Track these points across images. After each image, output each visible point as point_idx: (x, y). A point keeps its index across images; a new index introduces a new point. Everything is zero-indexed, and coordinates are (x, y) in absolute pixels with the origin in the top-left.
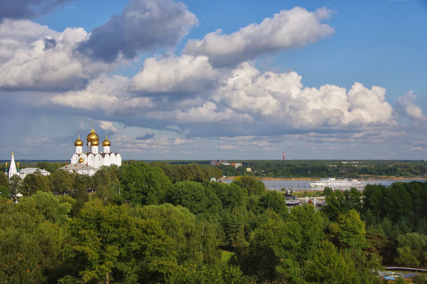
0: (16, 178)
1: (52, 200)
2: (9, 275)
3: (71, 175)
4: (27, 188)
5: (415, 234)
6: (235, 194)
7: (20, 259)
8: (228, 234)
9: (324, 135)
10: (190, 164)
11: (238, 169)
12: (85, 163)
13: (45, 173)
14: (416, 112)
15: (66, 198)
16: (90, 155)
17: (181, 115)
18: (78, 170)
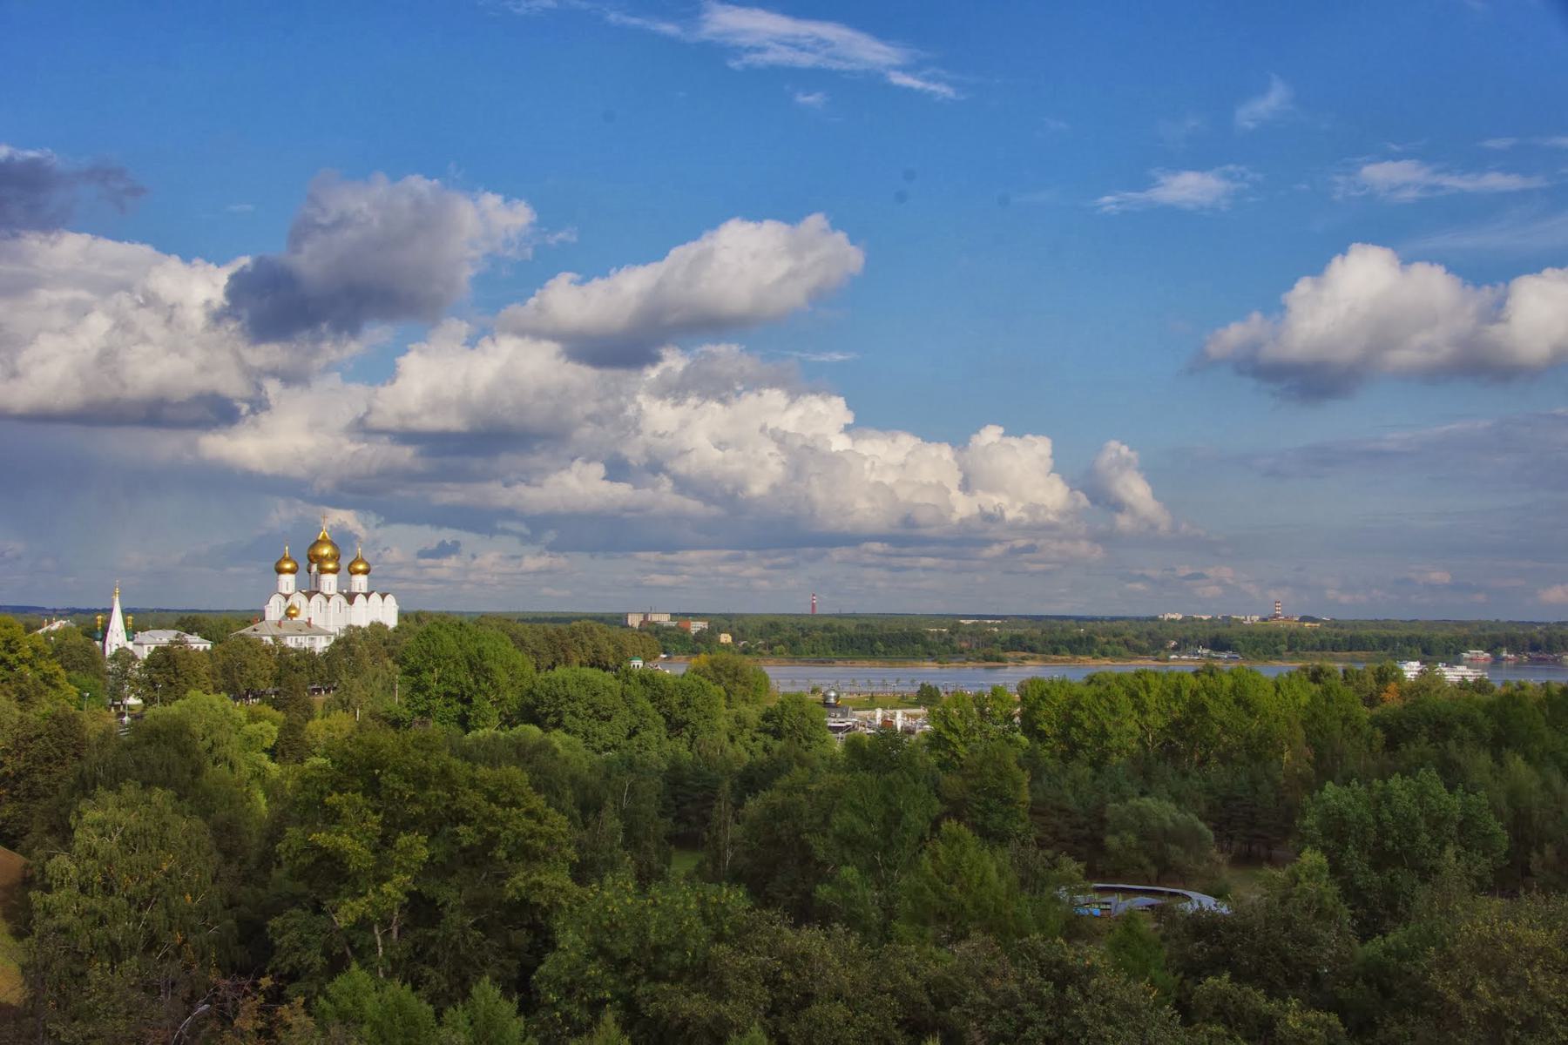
0: (124, 657)
1: (227, 714)
2: (140, 909)
3: (268, 651)
4: (153, 683)
5: (1147, 799)
6: (698, 701)
7: (165, 868)
8: (684, 804)
9: (907, 550)
10: (575, 624)
11: (699, 637)
12: (302, 617)
13: (197, 643)
14: (1136, 490)
15: (260, 708)
16: (316, 598)
17: (500, 495)
18: (285, 636)
